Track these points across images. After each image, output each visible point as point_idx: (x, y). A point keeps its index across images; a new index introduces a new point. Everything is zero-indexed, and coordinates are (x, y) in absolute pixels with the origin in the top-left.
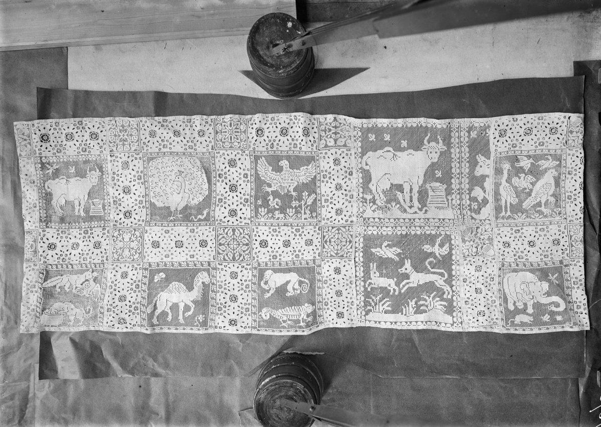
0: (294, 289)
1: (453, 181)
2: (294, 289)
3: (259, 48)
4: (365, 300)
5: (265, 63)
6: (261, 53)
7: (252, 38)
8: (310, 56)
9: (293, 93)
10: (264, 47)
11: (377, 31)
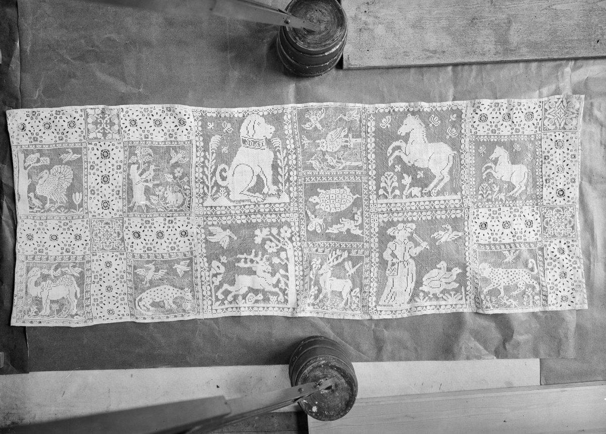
3: (346, 385)
6: (343, 380)
7: (353, 395)
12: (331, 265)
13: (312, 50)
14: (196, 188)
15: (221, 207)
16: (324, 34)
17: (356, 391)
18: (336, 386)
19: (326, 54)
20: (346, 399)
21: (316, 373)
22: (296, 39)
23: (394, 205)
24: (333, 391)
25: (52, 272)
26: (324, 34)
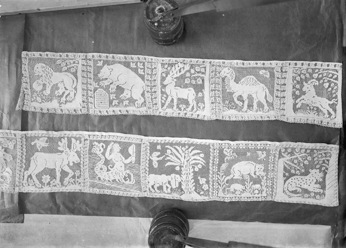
12: (174, 76)
13: (164, 227)
14: (261, 144)
16: (160, 237)
18: (166, 9)
19: (156, 226)
22: (175, 230)
23: (251, 145)
26: (160, 237)
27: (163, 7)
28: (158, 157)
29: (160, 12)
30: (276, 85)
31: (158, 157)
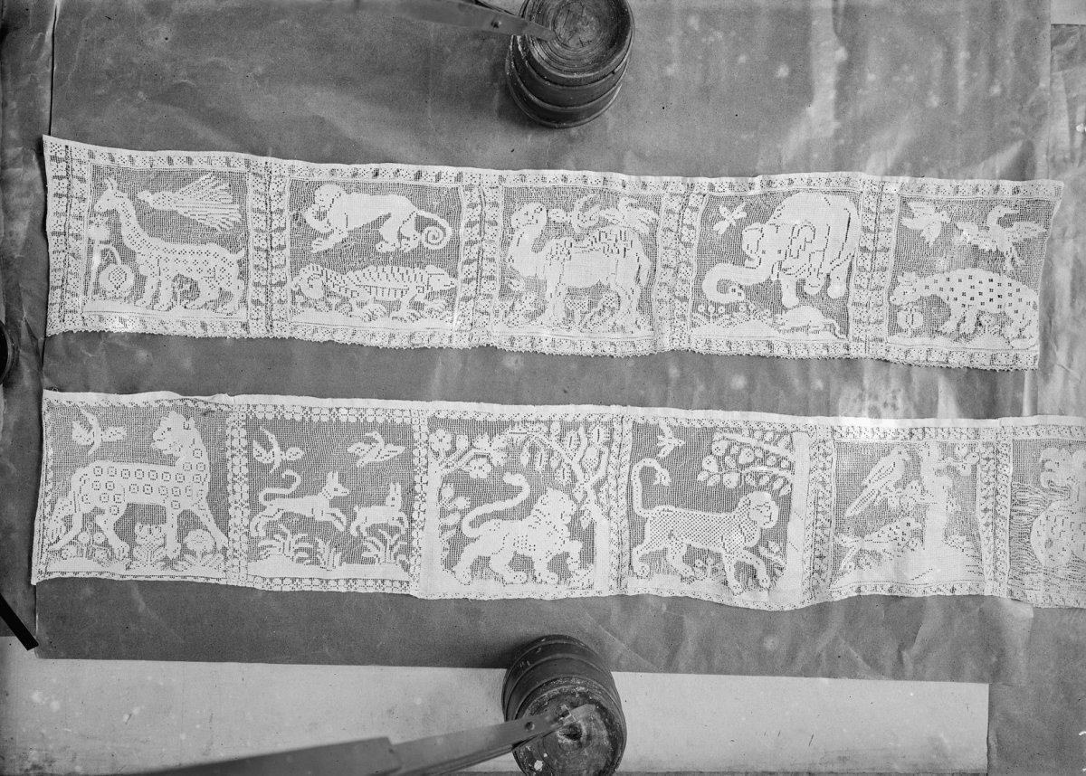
0: (400, 237)
1: (245, 470)
2: (400, 237)
3: (606, 743)
4: (410, 543)
5: (602, 710)
6: (605, 733)
7: (612, 763)
8: (511, 709)
9: (559, 641)
10: (595, 741)
11: (391, 751)
15: (365, 580)
17: (620, 759)
18: (589, 737)
20: (597, 766)
21: (675, 65)
24: (580, 745)
25: (574, 218)
27: (584, 728)
28: (268, 446)
29: (569, 736)
30: (86, 177)
31: (268, 446)
